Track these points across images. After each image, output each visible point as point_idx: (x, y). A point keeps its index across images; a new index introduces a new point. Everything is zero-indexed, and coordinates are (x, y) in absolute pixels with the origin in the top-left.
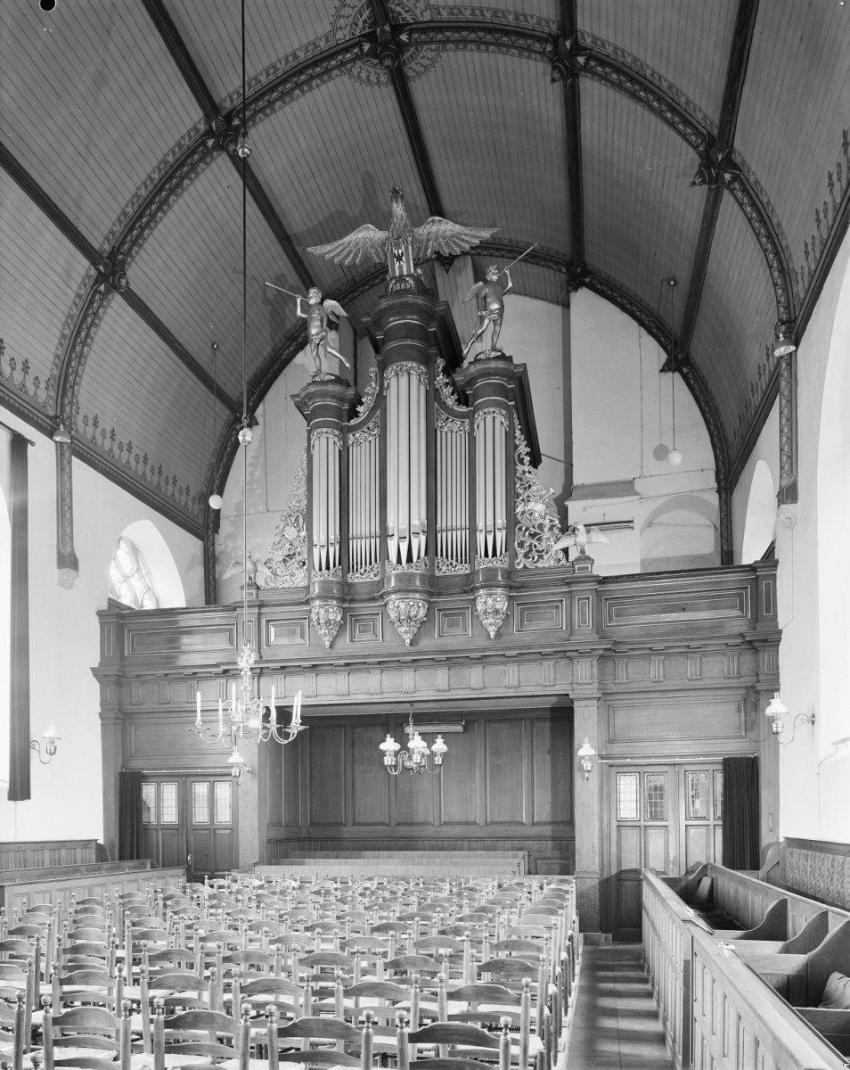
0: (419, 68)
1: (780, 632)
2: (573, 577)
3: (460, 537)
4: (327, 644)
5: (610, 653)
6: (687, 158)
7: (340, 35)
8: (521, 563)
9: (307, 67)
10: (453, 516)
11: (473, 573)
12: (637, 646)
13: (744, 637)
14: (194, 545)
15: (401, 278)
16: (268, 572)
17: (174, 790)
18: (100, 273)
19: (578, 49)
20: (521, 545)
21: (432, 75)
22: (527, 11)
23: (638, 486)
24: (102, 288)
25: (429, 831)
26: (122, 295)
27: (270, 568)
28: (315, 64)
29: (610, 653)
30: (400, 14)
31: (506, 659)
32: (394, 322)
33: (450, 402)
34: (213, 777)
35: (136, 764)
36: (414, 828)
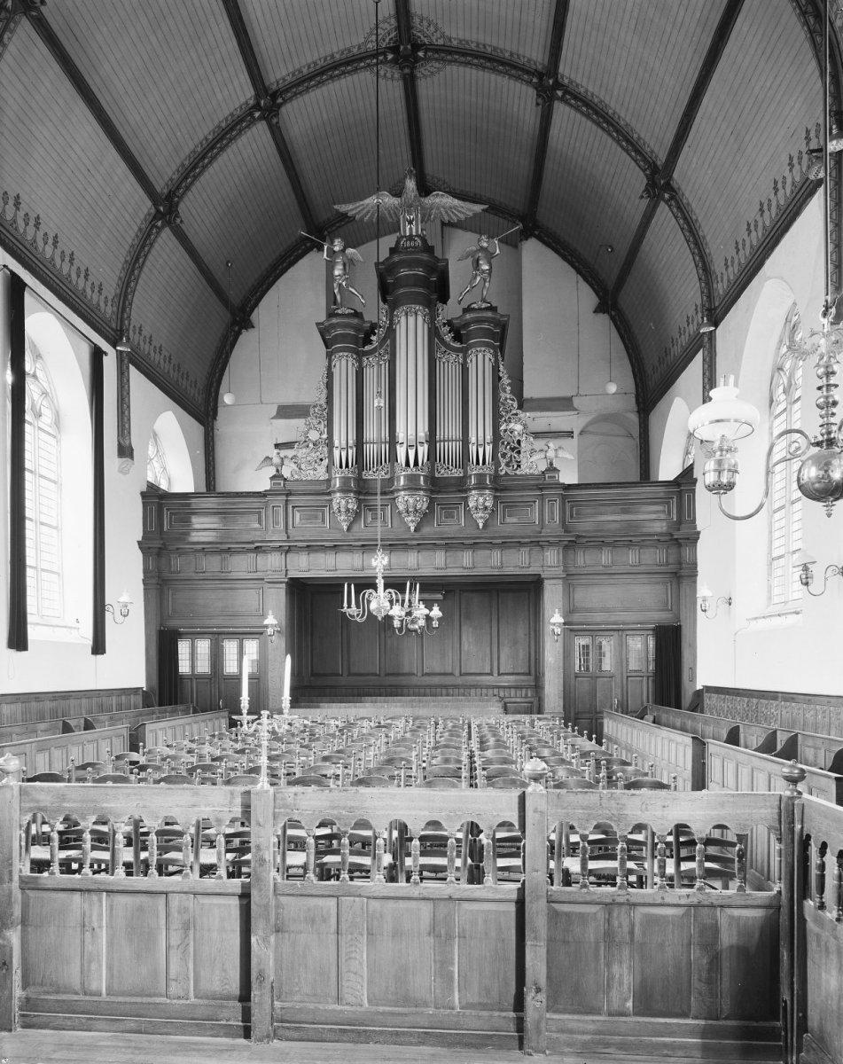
0: (426, 73)
1: (699, 533)
2: (545, 483)
3: (455, 448)
4: (345, 528)
5: (572, 543)
6: (638, 180)
7: (370, 45)
8: (503, 470)
9: (341, 65)
10: (449, 428)
11: (466, 477)
12: (592, 539)
13: (672, 535)
14: (197, 429)
15: (411, 238)
16: (294, 466)
17: (236, 646)
18: (158, 211)
19: (558, 85)
20: (504, 455)
21: (436, 78)
22: (521, 52)
23: (576, 402)
24: (159, 223)
25: (415, 680)
26: (172, 229)
27: (295, 463)
28: (348, 63)
29: (572, 543)
30: (420, 37)
31: (491, 546)
32: (404, 272)
33: (448, 338)
34: (241, 635)
35: (173, 623)
36: (401, 678)
